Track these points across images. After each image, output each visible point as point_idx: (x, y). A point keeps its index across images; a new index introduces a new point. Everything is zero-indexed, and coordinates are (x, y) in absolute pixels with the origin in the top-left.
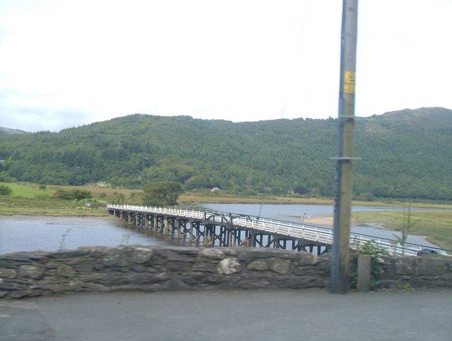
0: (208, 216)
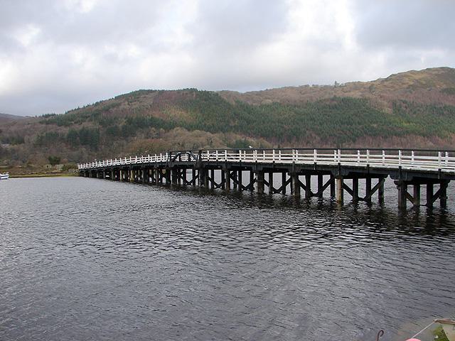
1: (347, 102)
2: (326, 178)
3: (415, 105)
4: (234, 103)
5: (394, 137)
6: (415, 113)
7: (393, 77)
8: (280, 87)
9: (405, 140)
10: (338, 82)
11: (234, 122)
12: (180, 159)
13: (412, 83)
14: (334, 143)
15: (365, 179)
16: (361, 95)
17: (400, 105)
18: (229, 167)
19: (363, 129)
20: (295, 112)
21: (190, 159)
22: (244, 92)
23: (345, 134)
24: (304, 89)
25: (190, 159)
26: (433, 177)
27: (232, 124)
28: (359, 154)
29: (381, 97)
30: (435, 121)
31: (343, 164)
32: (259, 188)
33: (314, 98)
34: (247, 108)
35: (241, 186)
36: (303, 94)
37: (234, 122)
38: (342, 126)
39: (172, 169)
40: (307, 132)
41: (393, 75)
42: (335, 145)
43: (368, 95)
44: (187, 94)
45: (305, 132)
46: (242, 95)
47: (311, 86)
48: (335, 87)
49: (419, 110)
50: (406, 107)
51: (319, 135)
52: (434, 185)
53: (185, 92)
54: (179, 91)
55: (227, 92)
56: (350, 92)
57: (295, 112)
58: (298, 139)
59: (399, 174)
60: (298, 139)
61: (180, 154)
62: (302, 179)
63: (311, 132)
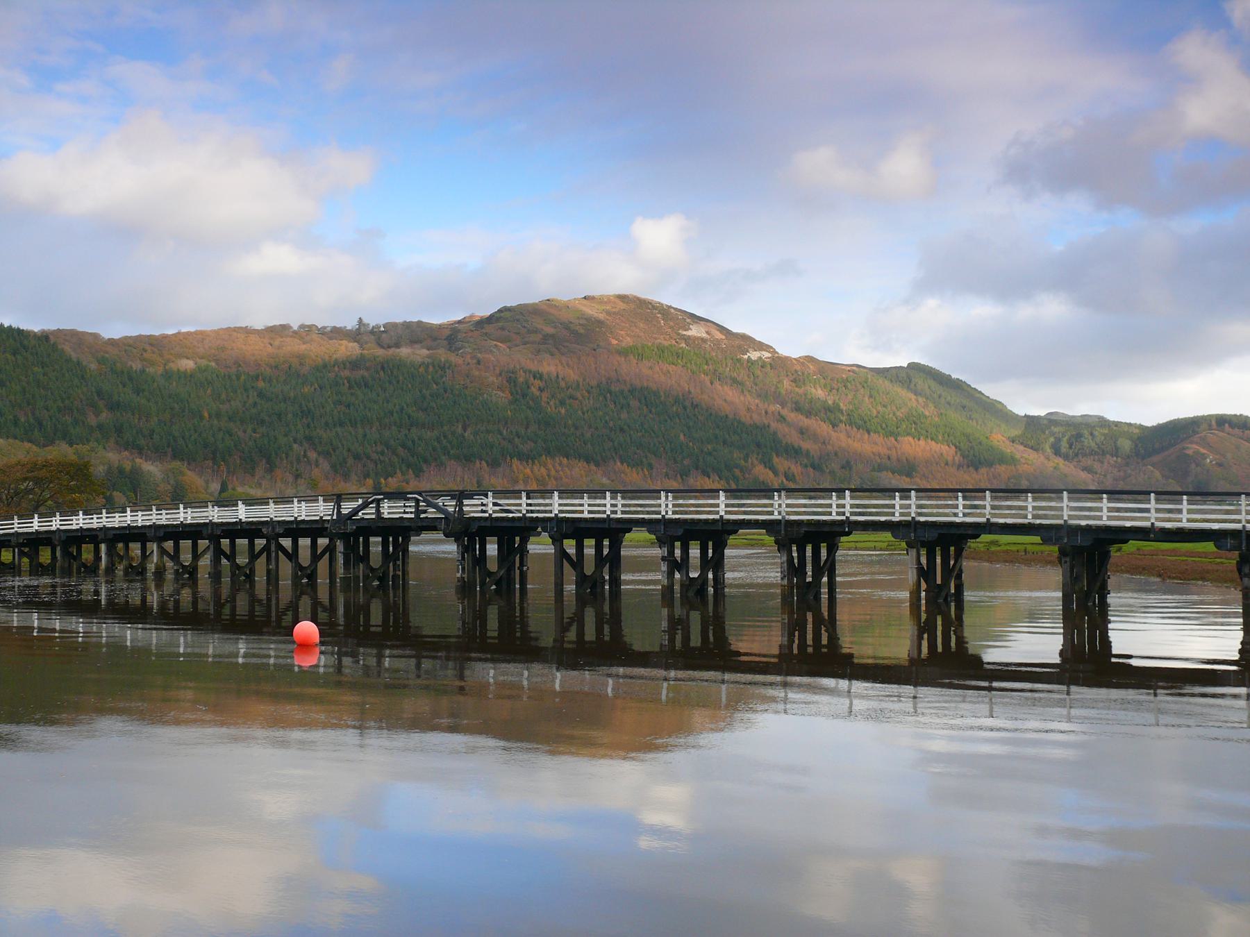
1: (390, 370)
2: (323, 542)
3: (563, 384)
4: (93, 366)
6: (562, 403)
7: (508, 314)
8: (113, 330)
10: (365, 321)
11: (97, 415)
13: (549, 330)
14: (367, 476)
15: (564, 540)
16: (428, 357)
17: (527, 382)
19: (438, 439)
20: (261, 395)
22: (790, 347)
23: (394, 452)
26: (838, 529)
27: (92, 420)
28: (154, 510)
29: (479, 363)
30: (611, 424)
32: (610, 547)
33: (118, 365)
34: (131, 379)
38: (387, 433)
42: (370, 482)
43: (443, 355)
45: (291, 448)
46: (112, 342)
47: (295, 328)
49: (571, 397)
50: (541, 390)
51: (326, 454)
52: (690, 542)
55: (73, 334)
56: (397, 345)
58: (271, 468)
60: (271, 468)
62: (286, 543)
63: (306, 445)
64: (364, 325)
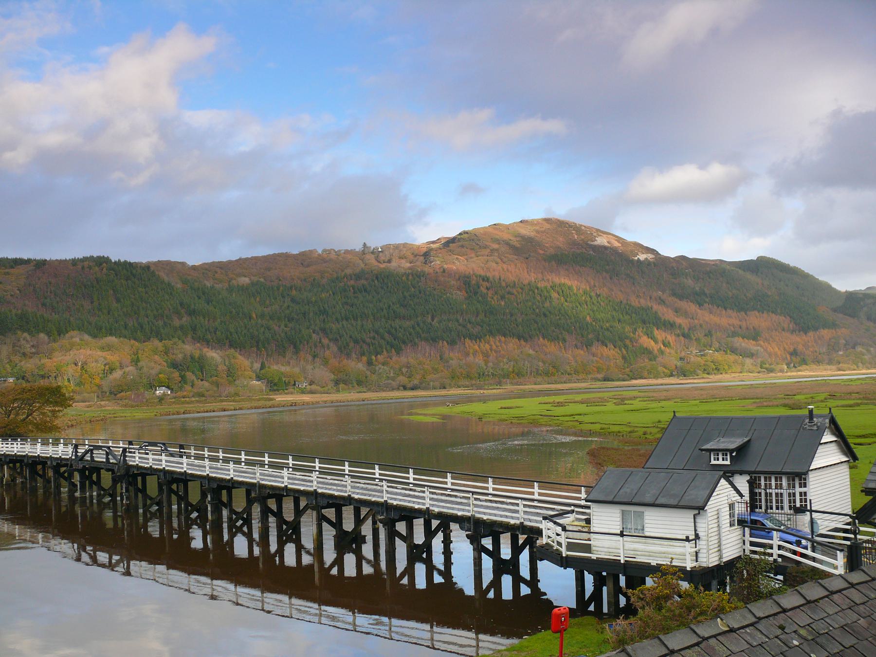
0: (81, 451)
3: (504, 284)
5: (467, 340)
6: (503, 298)
9: (487, 346)
10: (368, 245)
11: (180, 319)
12: (92, 457)
16: (410, 268)
18: (168, 477)
19: (414, 328)
21: (107, 459)
24: (304, 259)
25: (107, 459)
27: (177, 323)
31: (320, 491)
35: (188, 504)
36: (308, 266)
37: (180, 319)
39: (77, 470)
40: (314, 335)
41: (466, 233)
44: (90, 268)
45: (310, 337)
46: (194, 268)
47: (320, 252)
48: (363, 253)
50: (488, 289)
53: (86, 264)
54: (74, 262)
57: (293, 300)
59: (384, 509)
61: (92, 451)
63: (321, 335)
64: (367, 247)
